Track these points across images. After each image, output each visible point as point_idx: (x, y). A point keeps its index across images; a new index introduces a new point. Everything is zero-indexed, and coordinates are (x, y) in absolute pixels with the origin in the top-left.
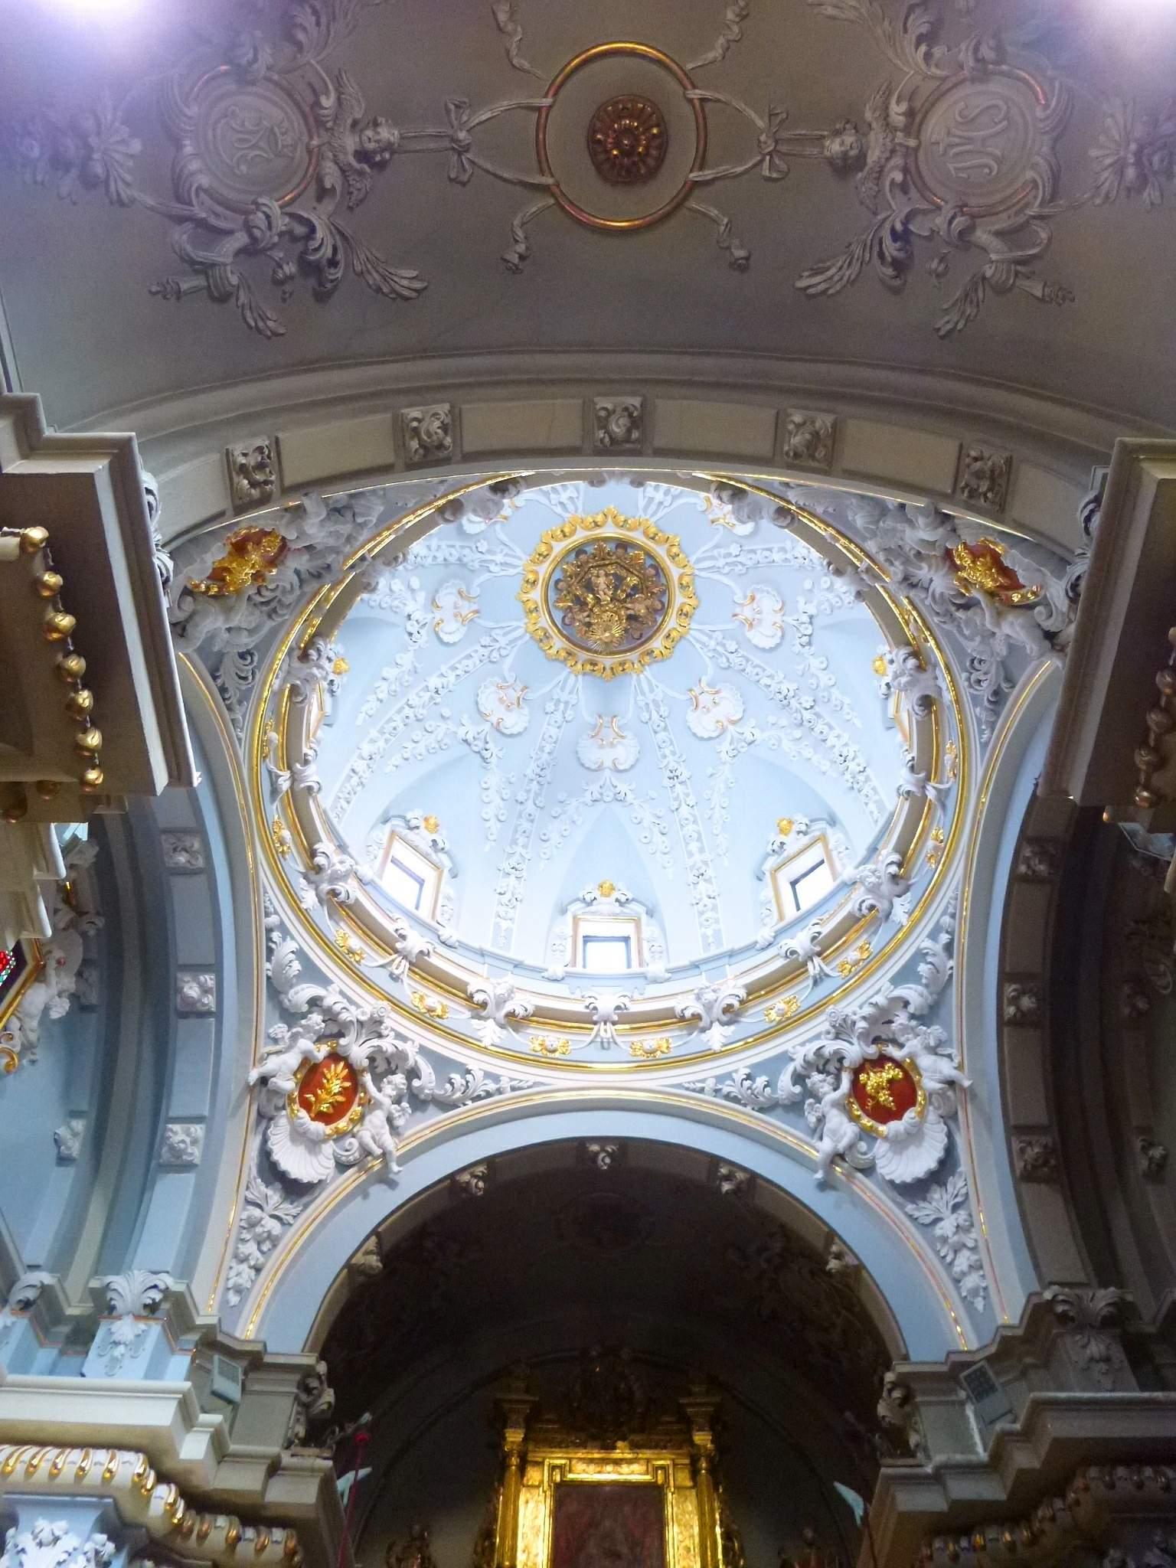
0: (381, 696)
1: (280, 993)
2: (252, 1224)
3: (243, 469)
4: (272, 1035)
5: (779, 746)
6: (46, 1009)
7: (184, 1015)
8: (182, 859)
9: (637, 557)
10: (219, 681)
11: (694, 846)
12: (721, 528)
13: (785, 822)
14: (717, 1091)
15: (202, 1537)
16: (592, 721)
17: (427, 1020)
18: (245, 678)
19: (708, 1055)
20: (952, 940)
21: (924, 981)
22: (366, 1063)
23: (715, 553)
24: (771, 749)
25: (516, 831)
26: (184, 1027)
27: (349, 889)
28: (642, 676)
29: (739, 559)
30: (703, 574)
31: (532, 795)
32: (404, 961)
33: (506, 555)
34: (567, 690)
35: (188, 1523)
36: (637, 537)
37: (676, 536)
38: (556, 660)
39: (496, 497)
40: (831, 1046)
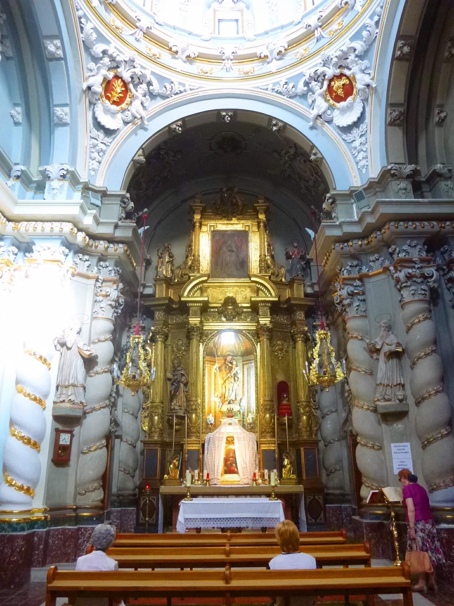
2: (95, 146)
4: (89, 68)
7: (51, 60)
15: (96, 247)
17: (153, 59)
20: (379, 19)
21: (364, 39)
22: (130, 79)
40: (321, 69)
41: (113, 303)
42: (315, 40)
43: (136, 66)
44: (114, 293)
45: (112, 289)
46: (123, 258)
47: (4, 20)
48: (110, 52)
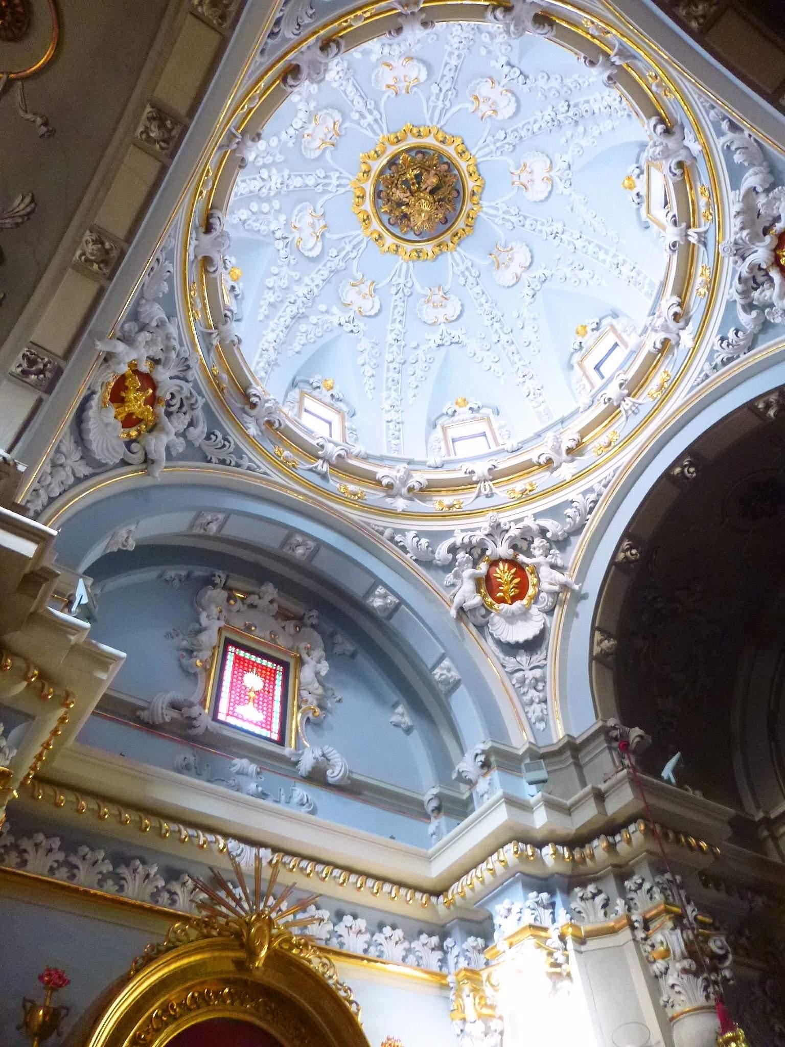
0: (370, 374)
1: (431, 562)
2: (523, 681)
3: (24, 372)
4: (448, 584)
5: (582, 148)
6: (317, 674)
7: (390, 617)
8: (300, 551)
9: (405, 160)
10: (213, 460)
11: (601, 255)
12: (415, 89)
13: (626, 182)
14: (715, 368)
15: (592, 856)
16: (487, 262)
17: (527, 497)
18: (224, 446)
19: (693, 352)
20: (730, 120)
21: (746, 164)
22: (511, 551)
23: (431, 104)
24: (580, 156)
25: (509, 358)
26: (394, 622)
27: (419, 478)
28: (484, 209)
29: (444, 90)
30: (442, 123)
31: (500, 331)
32: (486, 483)
33: (350, 242)
34: (460, 262)
35: (577, 856)
36: (392, 150)
37: (406, 125)
38: (437, 256)
39: (214, 234)
40: (743, 269)
41: (686, 963)
42: (702, 248)
43: (507, 527)
44: (674, 938)
45: (667, 932)
46: (654, 846)
47: (318, 617)
48: (459, 542)
